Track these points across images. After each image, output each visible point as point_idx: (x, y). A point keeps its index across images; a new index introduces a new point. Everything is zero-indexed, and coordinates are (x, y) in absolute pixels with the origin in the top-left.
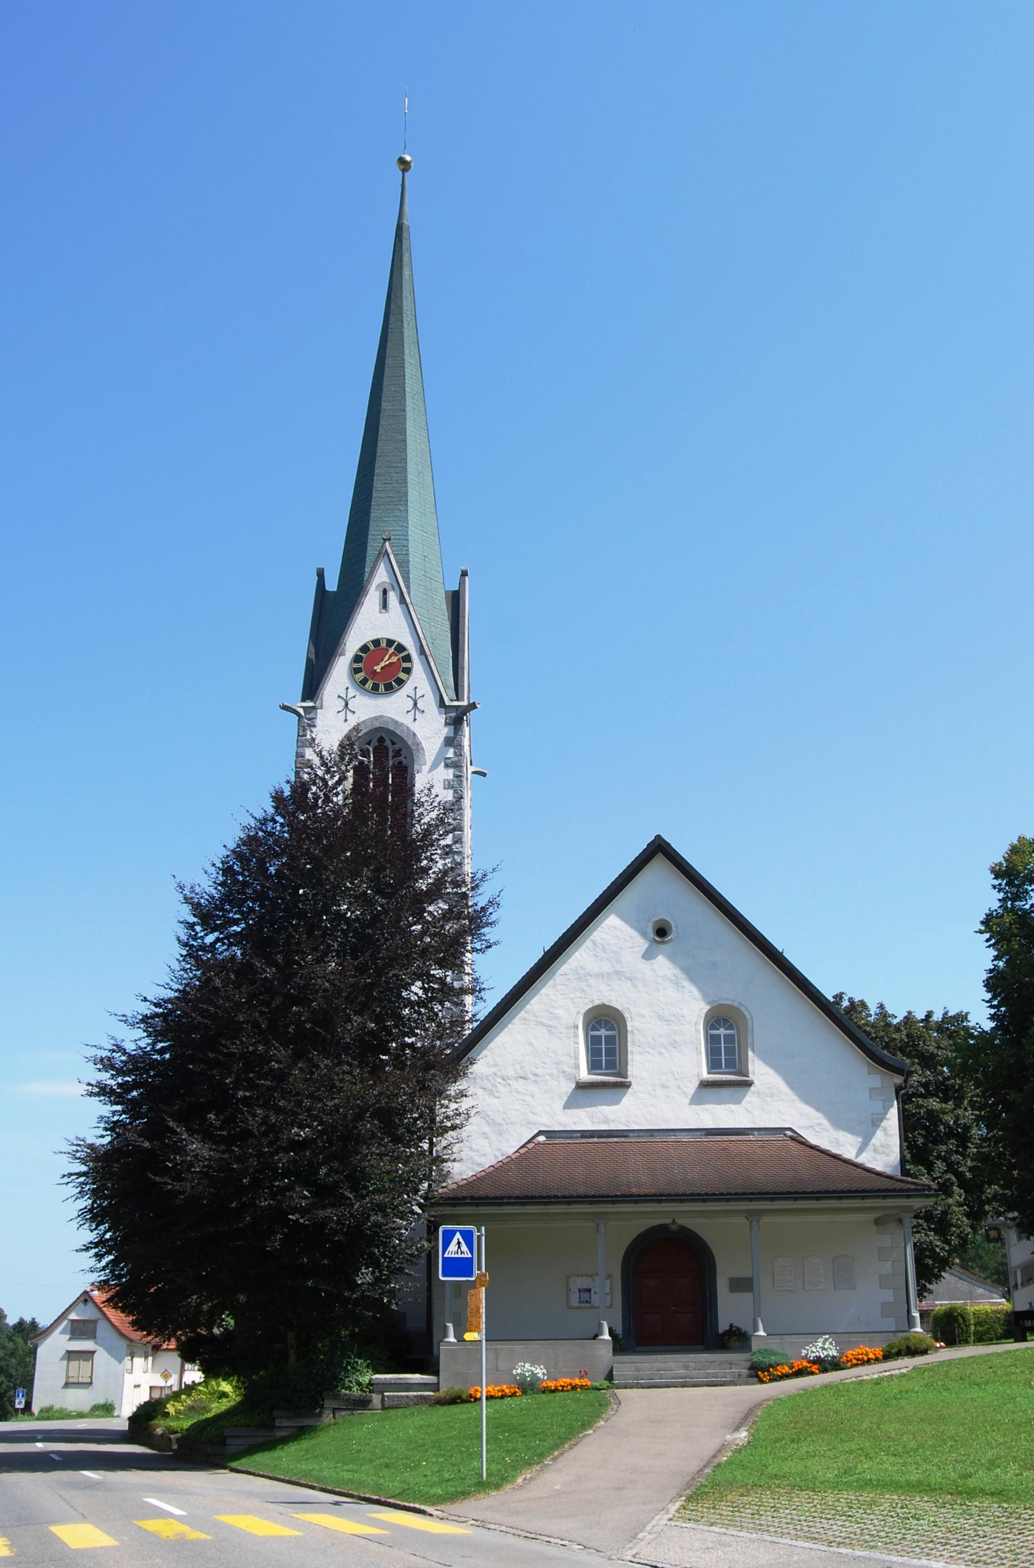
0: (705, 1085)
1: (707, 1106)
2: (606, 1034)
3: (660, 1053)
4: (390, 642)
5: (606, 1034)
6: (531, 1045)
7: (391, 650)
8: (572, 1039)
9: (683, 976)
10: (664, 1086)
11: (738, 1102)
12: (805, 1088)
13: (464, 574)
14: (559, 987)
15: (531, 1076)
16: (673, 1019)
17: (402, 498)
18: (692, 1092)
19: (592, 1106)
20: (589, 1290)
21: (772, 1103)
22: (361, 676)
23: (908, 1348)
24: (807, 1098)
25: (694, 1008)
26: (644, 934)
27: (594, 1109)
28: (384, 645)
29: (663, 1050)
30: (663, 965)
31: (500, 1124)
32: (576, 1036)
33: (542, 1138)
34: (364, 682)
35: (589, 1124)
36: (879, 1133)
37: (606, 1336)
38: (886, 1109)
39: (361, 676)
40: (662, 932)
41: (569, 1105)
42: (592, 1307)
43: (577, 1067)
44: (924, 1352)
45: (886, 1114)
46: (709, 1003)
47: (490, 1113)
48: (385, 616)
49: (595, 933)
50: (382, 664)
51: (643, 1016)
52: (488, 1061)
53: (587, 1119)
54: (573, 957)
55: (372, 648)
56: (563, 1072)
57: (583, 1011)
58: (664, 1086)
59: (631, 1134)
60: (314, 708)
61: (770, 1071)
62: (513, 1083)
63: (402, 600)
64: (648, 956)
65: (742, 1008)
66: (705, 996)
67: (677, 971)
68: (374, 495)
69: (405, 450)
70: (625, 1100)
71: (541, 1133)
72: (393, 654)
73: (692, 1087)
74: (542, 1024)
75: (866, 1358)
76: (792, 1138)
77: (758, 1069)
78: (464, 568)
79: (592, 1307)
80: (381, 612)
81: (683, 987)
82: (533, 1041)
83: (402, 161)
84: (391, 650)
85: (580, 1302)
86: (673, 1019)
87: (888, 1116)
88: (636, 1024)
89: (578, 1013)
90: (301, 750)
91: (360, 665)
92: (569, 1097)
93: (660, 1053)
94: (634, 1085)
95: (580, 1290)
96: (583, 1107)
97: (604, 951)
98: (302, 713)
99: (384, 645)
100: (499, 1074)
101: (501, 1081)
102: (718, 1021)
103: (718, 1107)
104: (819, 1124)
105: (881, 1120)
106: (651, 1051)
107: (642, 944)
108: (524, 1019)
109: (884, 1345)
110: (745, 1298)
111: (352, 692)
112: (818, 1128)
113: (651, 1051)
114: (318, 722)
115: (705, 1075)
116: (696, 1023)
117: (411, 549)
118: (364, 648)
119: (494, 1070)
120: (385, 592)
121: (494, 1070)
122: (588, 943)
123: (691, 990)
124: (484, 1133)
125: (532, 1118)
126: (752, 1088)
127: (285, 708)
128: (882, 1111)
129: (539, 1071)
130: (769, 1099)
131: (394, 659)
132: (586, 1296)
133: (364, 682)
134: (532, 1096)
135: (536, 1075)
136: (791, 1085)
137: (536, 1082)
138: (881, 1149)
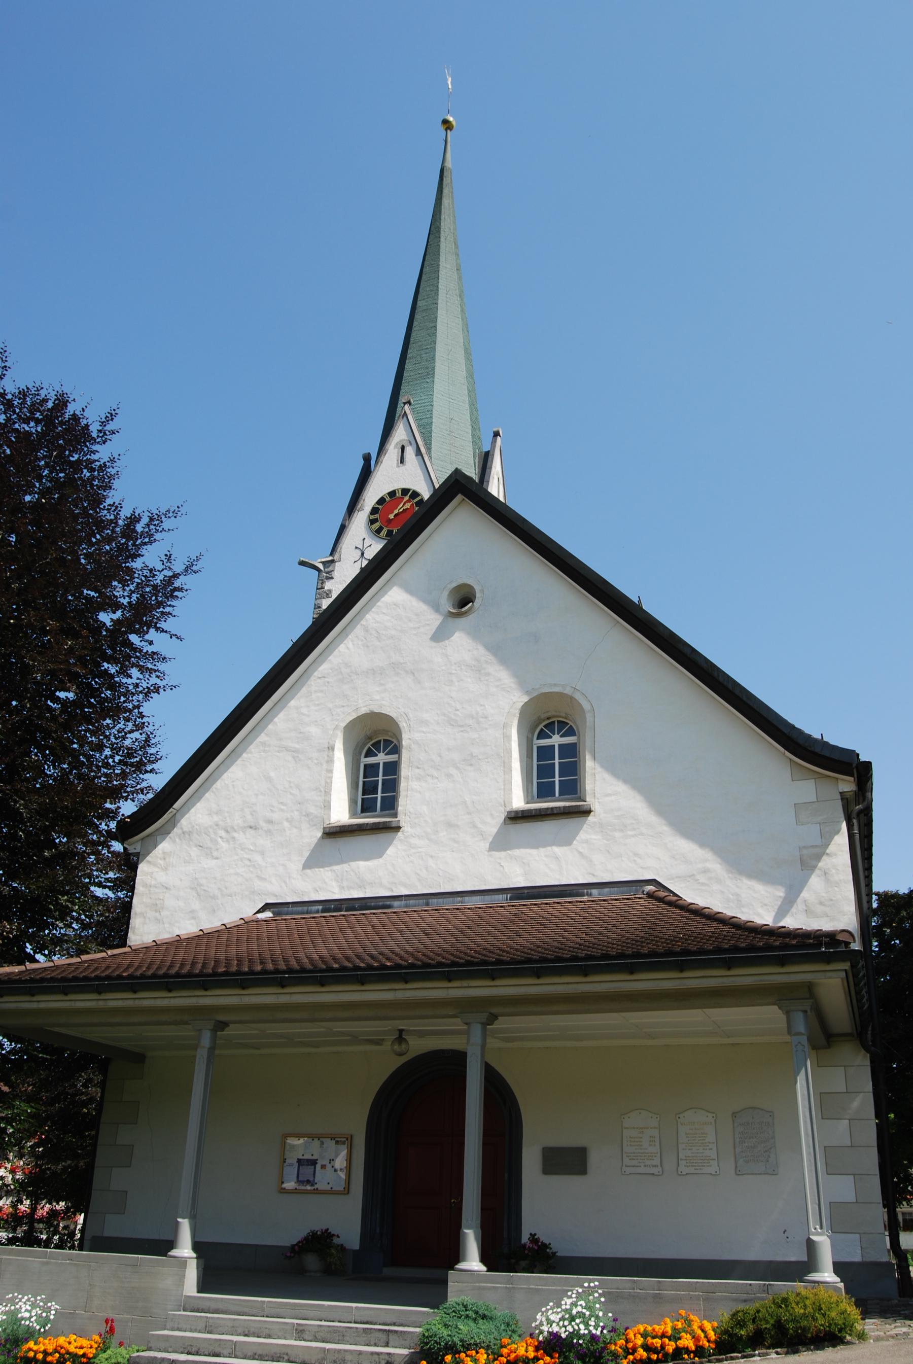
0: (517, 817)
1: (517, 852)
2: (377, 755)
3: (449, 776)
4: (405, 491)
5: (377, 755)
6: (269, 779)
7: (407, 498)
8: (325, 766)
9: (490, 657)
10: (450, 825)
11: (568, 842)
12: (680, 812)
13: (496, 434)
14: (314, 696)
15: (262, 824)
16: (470, 722)
17: (430, 373)
18: (494, 830)
19: (342, 862)
20: (313, 1163)
21: (629, 841)
22: (376, 526)
23: (779, 1325)
24: (684, 827)
25: (501, 705)
26: (436, 608)
27: (345, 867)
28: (399, 495)
29: (453, 771)
30: (462, 645)
31: (214, 897)
32: (331, 761)
33: (268, 914)
34: (379, 531)
35: (336, 890)
36: (815, 882)
37: (185, 1250)
38: (827, 839)
39: (376, 526)
40: (464, 600)
41: (314, 861)
42: (317, 1192)
43: (327, 806)
44: (831, 1338)
45: (827, 845)
46: (527, 693)
47: (203, 881)
48: (402, 468)
49: (368, 616)
50: (396, 512)
51: (425, 723)
52: (199, 812)
53: (334, 884)
54: (336, 652)
55: (388, 499)
56: (307, 815)
57: (343, 725)
58: (450, 825)
59: (396, 903)
60: (333, 561)
61: (621, 787)
62: (240, 837)
63: (418, 452)
64: (439, 636)
65: (578, 696)
66: (522, 684)
67: (481, 651)
68: (405, 374)
69: (435, 335)
70: (391, 851)
71: (266, 907)
72: (408, 501)
73: (494, 822)
74: (287, 749)
75: (670, 1347)
76: (650, 895)
77: (600, 785)
78: (495, 429)
79: (317, 1192)
80: (398, 466)
81: (489, 674)
82: (272, 774)
83: (445, 122)
84: (407, 498)
85: (299, 1181)
86: (470, 722)
87: (831, 848)
88: (417, 736)
89: (336, 728)
90: (318, 601)
91: (376, 516)
92: (313, 851)
93: (449, 776)
94: (406, 828)
95: (299, 1161)
96: (330, 865)
97: (378, 639)
98: (321, 566)
99: (399, 495)
100: (221, 823)
101: (223, 833)
102: (550, 726)
103: (534, 852)
104: (705, 871)
105: (819, 857)
106: (435, 774)
107: (434, 620)
108: (264, 744)
109: (724, 1314)
110: (565, 1185)
111: (368, 542)
112: (702, 879)
113: (435, 774)
114: (336, 574)
115: (518, 802)
116: (506, 726)
117: (435, 412)
118: (381, 501)
119: (216, 818)
120: (403, 448)
121: (216, 818)
122: (358, 631)
123: (504, 676)
124: (192, 911)
125: (258, 885)
126: (591, 818)
127: (302, 563)
128: (818, 842)
129: (275, 816)
130: (617, 834)
131: (408, 506)
132: (307, 1171)
133: (379, 531)
134: (262, 853)
135: (270, 822)
136: (659, 809)
137: (269, 832)
138: (819, 909)
